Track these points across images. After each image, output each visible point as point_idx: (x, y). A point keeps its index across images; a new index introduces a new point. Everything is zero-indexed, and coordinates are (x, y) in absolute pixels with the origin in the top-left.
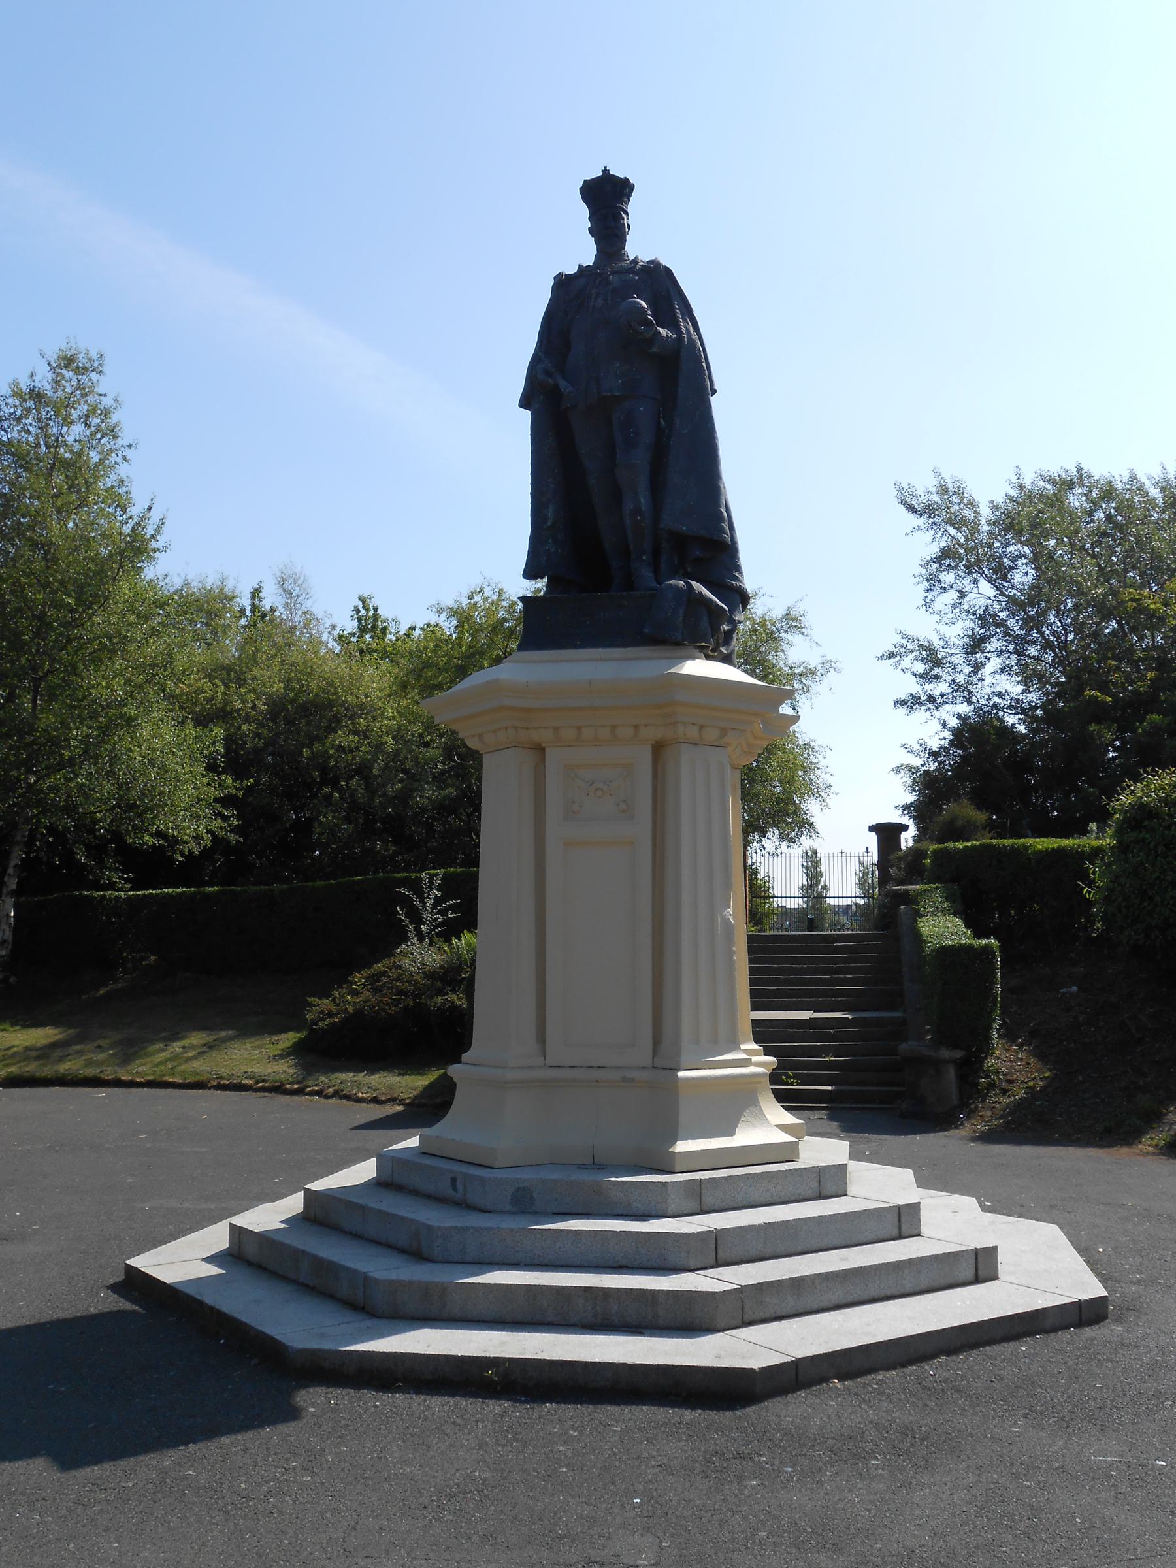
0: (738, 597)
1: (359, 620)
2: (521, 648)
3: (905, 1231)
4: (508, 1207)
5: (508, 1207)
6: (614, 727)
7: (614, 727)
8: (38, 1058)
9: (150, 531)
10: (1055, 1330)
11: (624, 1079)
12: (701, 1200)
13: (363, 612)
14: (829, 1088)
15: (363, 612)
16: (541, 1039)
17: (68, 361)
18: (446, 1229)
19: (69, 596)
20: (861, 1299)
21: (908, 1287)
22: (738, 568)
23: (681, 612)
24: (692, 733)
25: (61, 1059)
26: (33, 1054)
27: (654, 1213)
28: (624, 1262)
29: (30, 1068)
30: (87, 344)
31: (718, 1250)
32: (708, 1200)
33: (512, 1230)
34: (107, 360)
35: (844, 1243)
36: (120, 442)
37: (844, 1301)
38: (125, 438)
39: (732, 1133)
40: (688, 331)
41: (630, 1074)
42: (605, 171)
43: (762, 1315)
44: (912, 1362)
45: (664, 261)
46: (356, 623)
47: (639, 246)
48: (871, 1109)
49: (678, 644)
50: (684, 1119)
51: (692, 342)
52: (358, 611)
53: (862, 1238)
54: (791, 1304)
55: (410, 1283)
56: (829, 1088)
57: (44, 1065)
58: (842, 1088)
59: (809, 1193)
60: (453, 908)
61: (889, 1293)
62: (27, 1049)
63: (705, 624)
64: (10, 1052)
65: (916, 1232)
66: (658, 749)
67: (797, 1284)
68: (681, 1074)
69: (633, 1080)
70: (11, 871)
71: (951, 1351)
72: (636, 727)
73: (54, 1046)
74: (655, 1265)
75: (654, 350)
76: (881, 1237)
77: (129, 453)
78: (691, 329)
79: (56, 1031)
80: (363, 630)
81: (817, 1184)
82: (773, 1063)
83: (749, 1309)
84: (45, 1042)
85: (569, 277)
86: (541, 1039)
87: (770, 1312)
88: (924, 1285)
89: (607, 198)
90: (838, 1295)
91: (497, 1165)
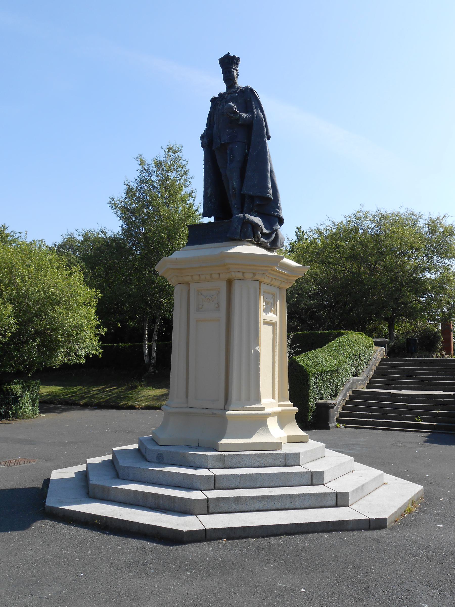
0: (277, 219)
1: (297, 236)
2: (188, 244)
3: (314, 482)
4: (155, 461)
5: (155, 461)
6: (211, 274)
7: (211, 274)
8: (157, 399)
9: (195, 208)
10: (353, 530)
11: (213, 414)
12: (223, 463)
13: (298, 233)
14: (434, 424)
15: (298, 233)
16: (187, 396)
17: (170, 149)
18: (123, 467)
19: (164, 234)
20: (271, 508)
21: (297, 505)
22: (279, 208)
23: (240, 227)
24: (240, 275)
25: (164, 400)
26: (156, 398)
27: (203, 467)
28: (179, 485)
29: (153, 403)
30: (175, 142)
31: (215, 483)
32: (228, 463)
33: (144, 469)
34: (183, 148)
35: (281, 485)
36: (188, 177)
37: (262, 509)
38: (190, 174)
39: (250, 437)
40: (257, 113)
41: (215, 412)
42: (229, 54)
43: (219, 511)
44: (268, 536)
45: (250, 86)
46: (296, 238)
47: (241, 83)
48: (439, 433)
49: (240, 240)
50: (228, 431)
51: (258, 117)
52: (297, 233)
53: (291, 484)
54: (234, 507)
55: (99, 485)
56: (434, 424)
57: (158, 402)
58: (439, 424)
59: (279, 464)
60: (298, 347)
61: (287, 507)
62: (155, 396)
63: (250, 231)
64: (148, 397)
65: (321, 483)
66: (230, 283)
67: (237, 500)
68: (228, 412)
69: (216, 414)
70: (155, 333)
71: (289, 534)
72: (219, 274)
73: (163, 395)
74: (189, 487)
75: (240, 122)
76: (301, 484)
77: (191, 181)
78: (259, 112)
79: (166, 390)
80: (299, 240)
81: (284, 460)
82: (296, 410)
83: (209, 507)
84: (161, 394)
85: (215, 98)
86: (187, 396)
87: (222, 510)
88: (307, 505)
89: (229, 64)
90: (259, 505)
91: (160, 444)
